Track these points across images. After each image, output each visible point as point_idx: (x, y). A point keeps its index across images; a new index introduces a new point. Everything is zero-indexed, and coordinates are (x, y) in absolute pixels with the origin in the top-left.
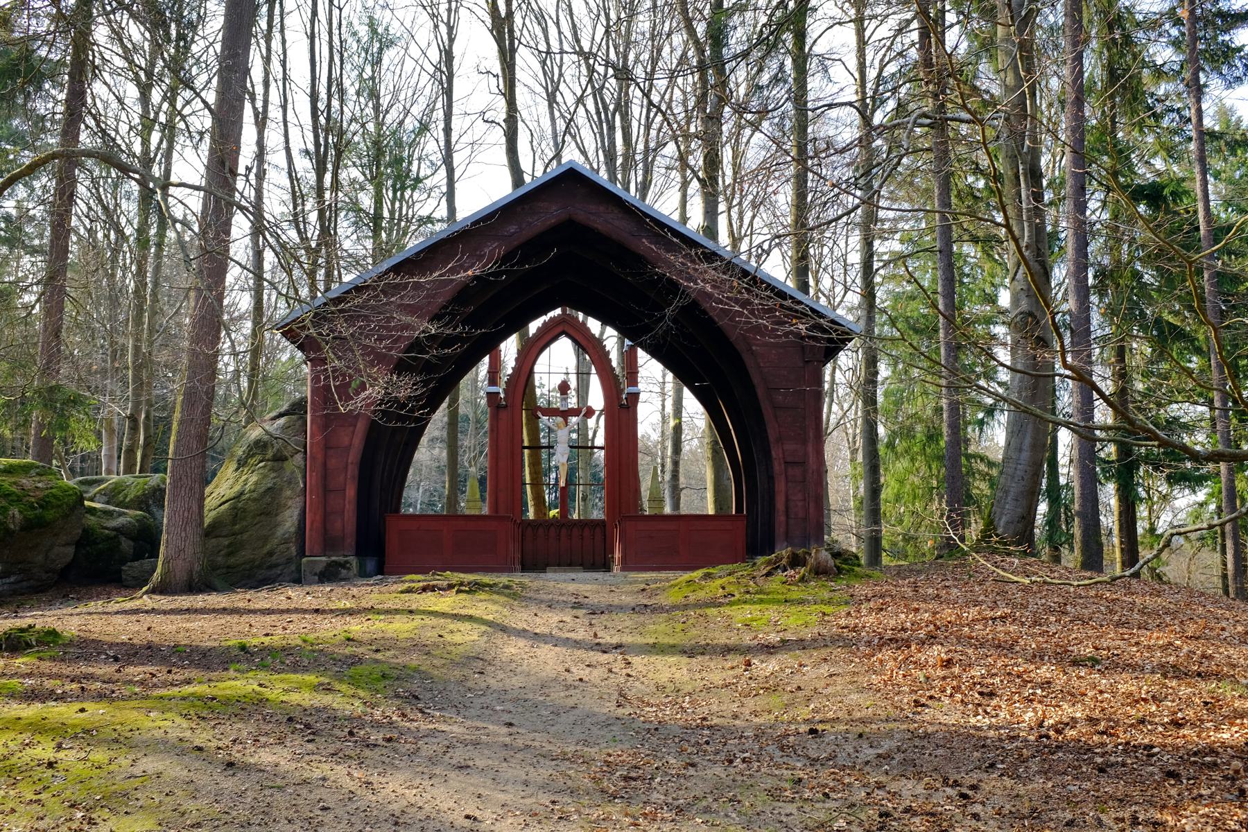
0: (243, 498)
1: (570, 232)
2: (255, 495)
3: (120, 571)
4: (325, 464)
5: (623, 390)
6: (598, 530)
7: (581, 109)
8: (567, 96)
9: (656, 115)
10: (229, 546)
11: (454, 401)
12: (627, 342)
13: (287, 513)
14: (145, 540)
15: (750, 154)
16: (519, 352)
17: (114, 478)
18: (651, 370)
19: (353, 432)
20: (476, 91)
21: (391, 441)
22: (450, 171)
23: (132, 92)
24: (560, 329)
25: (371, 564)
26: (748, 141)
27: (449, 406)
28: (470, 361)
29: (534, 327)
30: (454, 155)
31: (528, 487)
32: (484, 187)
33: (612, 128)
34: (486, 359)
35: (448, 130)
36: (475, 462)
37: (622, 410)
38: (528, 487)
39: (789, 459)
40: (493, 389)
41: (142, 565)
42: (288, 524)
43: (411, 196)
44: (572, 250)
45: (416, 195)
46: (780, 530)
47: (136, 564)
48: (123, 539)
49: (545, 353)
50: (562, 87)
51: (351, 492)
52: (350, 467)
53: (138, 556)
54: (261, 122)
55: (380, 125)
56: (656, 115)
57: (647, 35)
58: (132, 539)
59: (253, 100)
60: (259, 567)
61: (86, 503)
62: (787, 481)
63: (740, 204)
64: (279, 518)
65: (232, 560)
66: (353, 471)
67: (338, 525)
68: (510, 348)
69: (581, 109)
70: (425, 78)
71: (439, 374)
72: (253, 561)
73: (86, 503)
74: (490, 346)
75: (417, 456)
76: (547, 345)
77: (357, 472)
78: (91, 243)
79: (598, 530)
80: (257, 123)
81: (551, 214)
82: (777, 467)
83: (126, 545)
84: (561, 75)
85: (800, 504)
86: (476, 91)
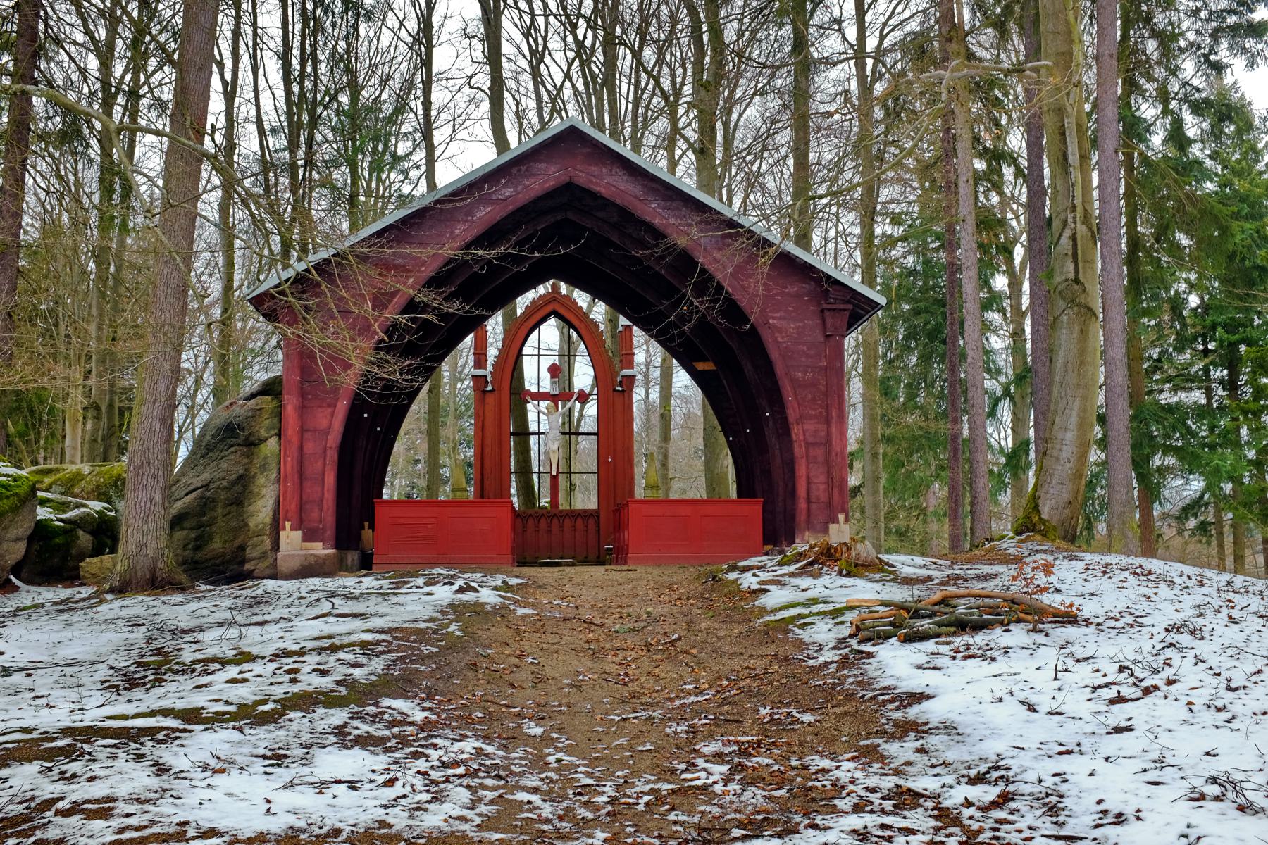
0: (212, 486)
1: (570, 194)
2: (225, 483)
3: (77, 568)
4: (301, 448)
5: (618, 374)
6: (591, 521)
7: (568, 84)
8: (554, 70)
9: (653, 69)
10: (196, 539)
11: (434, 392)
12: (623, 321)
13: (260, 503)
14: (105, 534)
15: (739, 135)
16: (506, 332)
17: (74, 468)
18: (646, 351)
19: (332, 416)
20: (455, 57)
21: (371, 427)
22: (430, 148)
23: (93, 63)
24: (549, 308)
25: (352, 557)
26: (736, 124)
27: (430, 391)
28: (449, 344)
29: (524, 301)
30: (435, 132)
31: (513, 477)
32: (466, 153)
33: (600, 101)
34: (469, 339)
35: (427, 104)
36: (460, 451)
37: (614, 390)
38: (513, 477)
39: (811, 440)
40: (480, 372)
41: (101, 561)
42: (262, 515)
43: (388, 177)
44: (572, 225)
45: (393, 175)
46: (801, 517)
47: (95, 560)
48: (81, 533)
49: (535, 334)
50: (547, 59)
51: (330, 479)
52: (329, 453)
53: (97, 551)
54: (230, 94)
55: (355, 98)
56: (653, 69)
57: (635, 8)
58: (91, 533)
59: (221, 65)
60: (229, 562)
61: (39, 494)
62: (808, 463)
63: (729, 185)
64: (251, 508)
65: (199, 556)
66: (332, 455)
67: (315, 515)
68: (495, 326)
69: (568, 84)
70: (403, 48)
71: (426, 343)
72: (223, 555)
73: (39, 494)
74: (475, 323)
75: (395, 449)
76: (537, 325)
77: (336, 457)
78: (50, 228)
79: (591, 521)
80: (225, 92)
81: (547, 177)
82: (799, 450)
83: (84, 539)
84: (545, 46)
85: (822, 487)
86: (455, 57)
